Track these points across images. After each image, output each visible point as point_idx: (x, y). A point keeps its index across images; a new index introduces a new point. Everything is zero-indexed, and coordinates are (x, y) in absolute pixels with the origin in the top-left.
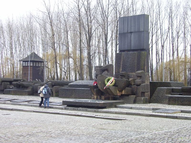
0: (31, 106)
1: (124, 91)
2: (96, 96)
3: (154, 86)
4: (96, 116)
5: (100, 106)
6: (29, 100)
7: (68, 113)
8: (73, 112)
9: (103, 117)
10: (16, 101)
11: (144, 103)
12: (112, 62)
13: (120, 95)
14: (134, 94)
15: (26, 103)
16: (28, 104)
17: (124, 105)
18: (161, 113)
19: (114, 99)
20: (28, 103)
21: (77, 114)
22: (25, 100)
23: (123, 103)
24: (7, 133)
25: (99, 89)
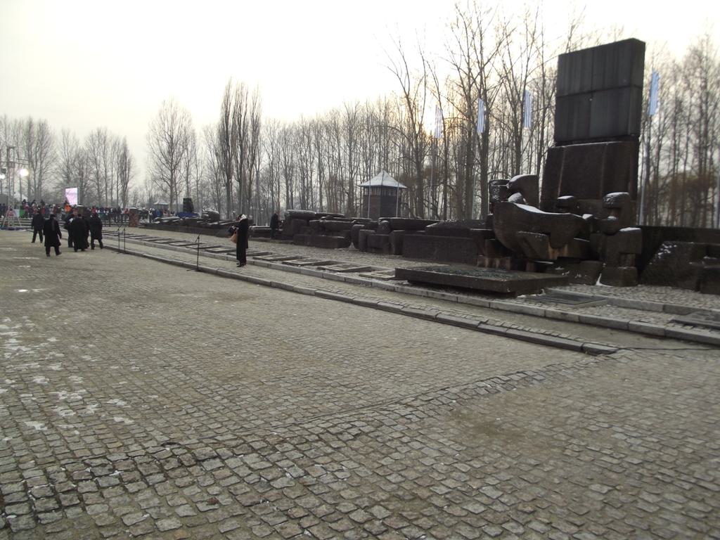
0: (370, 285)
1: (566, 248)
2: (489, 257)
3: (653, 236)
4: (483, 326)
5: (495, 288)
6: (364, 266)
7: (400, 307)
8: (432, 308)
9: (502, 330)
10: (264, 257)
11: (698, 288)
12: (703, 163)
13: (556, 258)
14: (596, 258)
15: (314, 269)
16: (360, 278)
17: (568, 290)
18: (694, 325)
19: (541, 269)
20: (360, 276)
21: (423, 312)
22: (317, 260)
23: (564, 282)
24: (173, 323)
25: (497, 241)
